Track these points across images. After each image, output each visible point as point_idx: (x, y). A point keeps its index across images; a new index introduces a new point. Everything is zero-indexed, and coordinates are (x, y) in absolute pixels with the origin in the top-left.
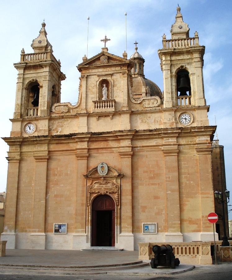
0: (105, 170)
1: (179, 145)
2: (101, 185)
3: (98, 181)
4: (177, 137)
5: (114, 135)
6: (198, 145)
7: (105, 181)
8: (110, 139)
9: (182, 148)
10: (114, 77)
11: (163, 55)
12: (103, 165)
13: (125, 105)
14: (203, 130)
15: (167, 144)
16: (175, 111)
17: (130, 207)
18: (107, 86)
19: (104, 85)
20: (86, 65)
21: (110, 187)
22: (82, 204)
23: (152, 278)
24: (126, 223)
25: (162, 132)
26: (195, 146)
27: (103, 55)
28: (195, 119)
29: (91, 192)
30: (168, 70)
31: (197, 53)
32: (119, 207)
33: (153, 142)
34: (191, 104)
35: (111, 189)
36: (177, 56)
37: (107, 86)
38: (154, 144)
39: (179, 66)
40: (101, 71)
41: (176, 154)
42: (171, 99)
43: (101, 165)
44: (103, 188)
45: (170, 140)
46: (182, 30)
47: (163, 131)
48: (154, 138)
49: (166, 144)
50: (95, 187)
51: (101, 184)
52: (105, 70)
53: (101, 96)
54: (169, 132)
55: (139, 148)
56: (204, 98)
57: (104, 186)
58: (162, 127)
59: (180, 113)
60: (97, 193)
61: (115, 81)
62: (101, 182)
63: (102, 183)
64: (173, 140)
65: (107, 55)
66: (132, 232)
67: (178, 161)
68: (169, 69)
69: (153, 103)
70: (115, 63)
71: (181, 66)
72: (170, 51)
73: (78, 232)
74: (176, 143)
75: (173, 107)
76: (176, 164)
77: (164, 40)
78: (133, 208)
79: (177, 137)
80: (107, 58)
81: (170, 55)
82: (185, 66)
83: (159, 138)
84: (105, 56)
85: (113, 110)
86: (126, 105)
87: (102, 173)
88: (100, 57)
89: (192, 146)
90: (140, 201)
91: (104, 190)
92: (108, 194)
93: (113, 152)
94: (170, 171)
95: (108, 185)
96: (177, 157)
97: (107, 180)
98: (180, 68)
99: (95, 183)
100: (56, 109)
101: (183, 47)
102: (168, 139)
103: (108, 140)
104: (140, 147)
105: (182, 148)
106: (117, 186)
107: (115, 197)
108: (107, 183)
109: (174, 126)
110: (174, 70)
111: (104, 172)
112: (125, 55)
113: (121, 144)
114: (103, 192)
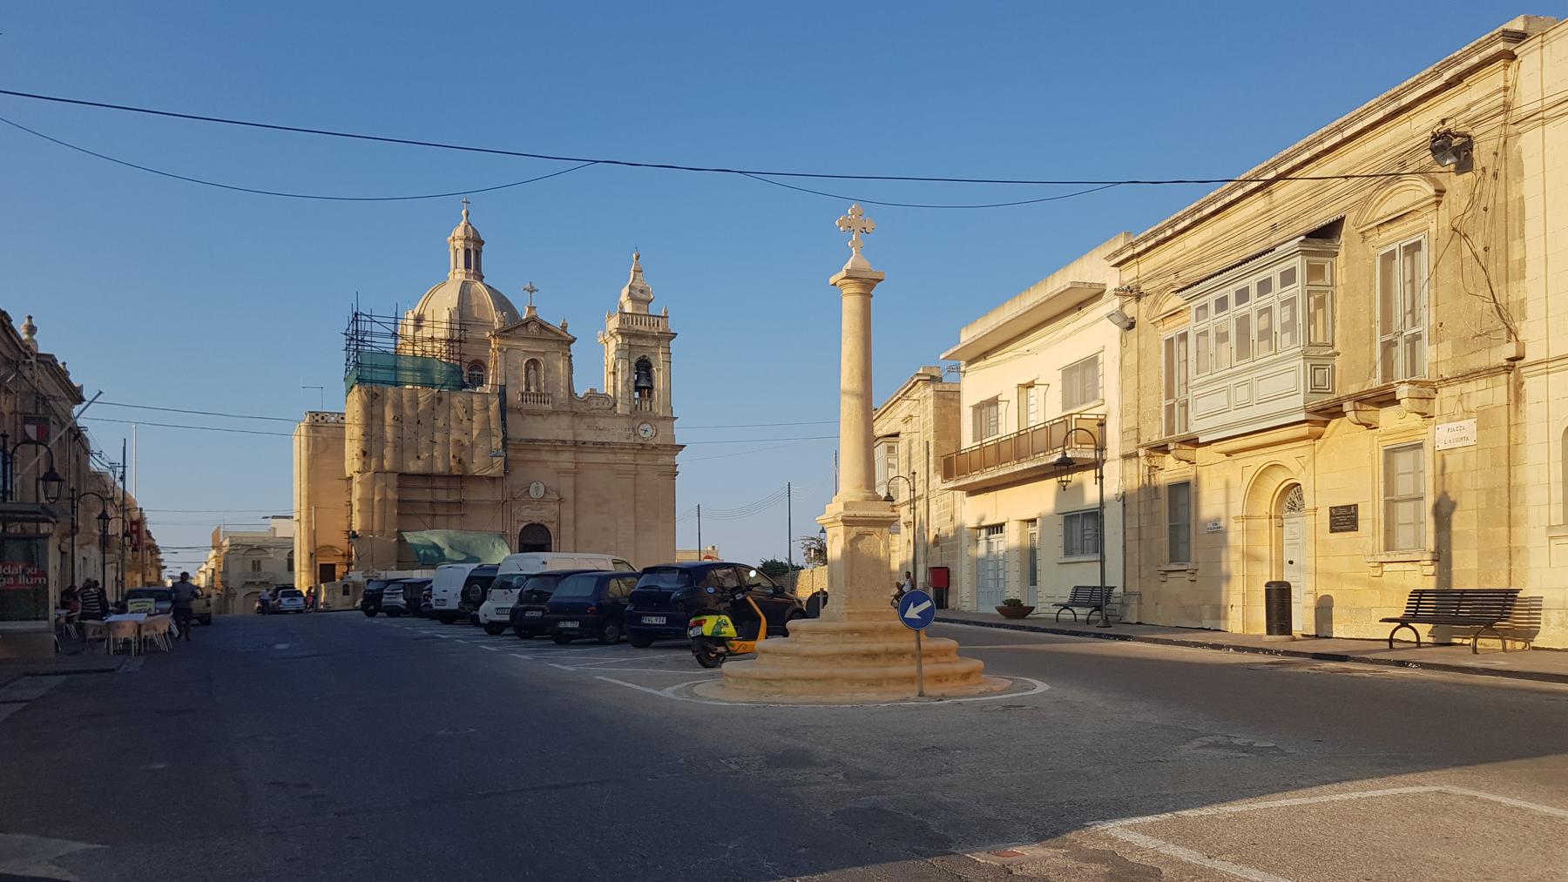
1: (637, 465)
4: (635, 454)
7: (539, 507)
19: (532, 367)
20: (505, 331)
21: (547, 514)
46: (643, 296)
52: (534, 343)
59: (639, 422)
64: (628, 458)
70: (552, 336)
79: (635, 454)
85: (551, 408)
92: (543, 523)
101: (648, 329)
107: (552, 528)
110: (634, 361)
114: (536, 520)
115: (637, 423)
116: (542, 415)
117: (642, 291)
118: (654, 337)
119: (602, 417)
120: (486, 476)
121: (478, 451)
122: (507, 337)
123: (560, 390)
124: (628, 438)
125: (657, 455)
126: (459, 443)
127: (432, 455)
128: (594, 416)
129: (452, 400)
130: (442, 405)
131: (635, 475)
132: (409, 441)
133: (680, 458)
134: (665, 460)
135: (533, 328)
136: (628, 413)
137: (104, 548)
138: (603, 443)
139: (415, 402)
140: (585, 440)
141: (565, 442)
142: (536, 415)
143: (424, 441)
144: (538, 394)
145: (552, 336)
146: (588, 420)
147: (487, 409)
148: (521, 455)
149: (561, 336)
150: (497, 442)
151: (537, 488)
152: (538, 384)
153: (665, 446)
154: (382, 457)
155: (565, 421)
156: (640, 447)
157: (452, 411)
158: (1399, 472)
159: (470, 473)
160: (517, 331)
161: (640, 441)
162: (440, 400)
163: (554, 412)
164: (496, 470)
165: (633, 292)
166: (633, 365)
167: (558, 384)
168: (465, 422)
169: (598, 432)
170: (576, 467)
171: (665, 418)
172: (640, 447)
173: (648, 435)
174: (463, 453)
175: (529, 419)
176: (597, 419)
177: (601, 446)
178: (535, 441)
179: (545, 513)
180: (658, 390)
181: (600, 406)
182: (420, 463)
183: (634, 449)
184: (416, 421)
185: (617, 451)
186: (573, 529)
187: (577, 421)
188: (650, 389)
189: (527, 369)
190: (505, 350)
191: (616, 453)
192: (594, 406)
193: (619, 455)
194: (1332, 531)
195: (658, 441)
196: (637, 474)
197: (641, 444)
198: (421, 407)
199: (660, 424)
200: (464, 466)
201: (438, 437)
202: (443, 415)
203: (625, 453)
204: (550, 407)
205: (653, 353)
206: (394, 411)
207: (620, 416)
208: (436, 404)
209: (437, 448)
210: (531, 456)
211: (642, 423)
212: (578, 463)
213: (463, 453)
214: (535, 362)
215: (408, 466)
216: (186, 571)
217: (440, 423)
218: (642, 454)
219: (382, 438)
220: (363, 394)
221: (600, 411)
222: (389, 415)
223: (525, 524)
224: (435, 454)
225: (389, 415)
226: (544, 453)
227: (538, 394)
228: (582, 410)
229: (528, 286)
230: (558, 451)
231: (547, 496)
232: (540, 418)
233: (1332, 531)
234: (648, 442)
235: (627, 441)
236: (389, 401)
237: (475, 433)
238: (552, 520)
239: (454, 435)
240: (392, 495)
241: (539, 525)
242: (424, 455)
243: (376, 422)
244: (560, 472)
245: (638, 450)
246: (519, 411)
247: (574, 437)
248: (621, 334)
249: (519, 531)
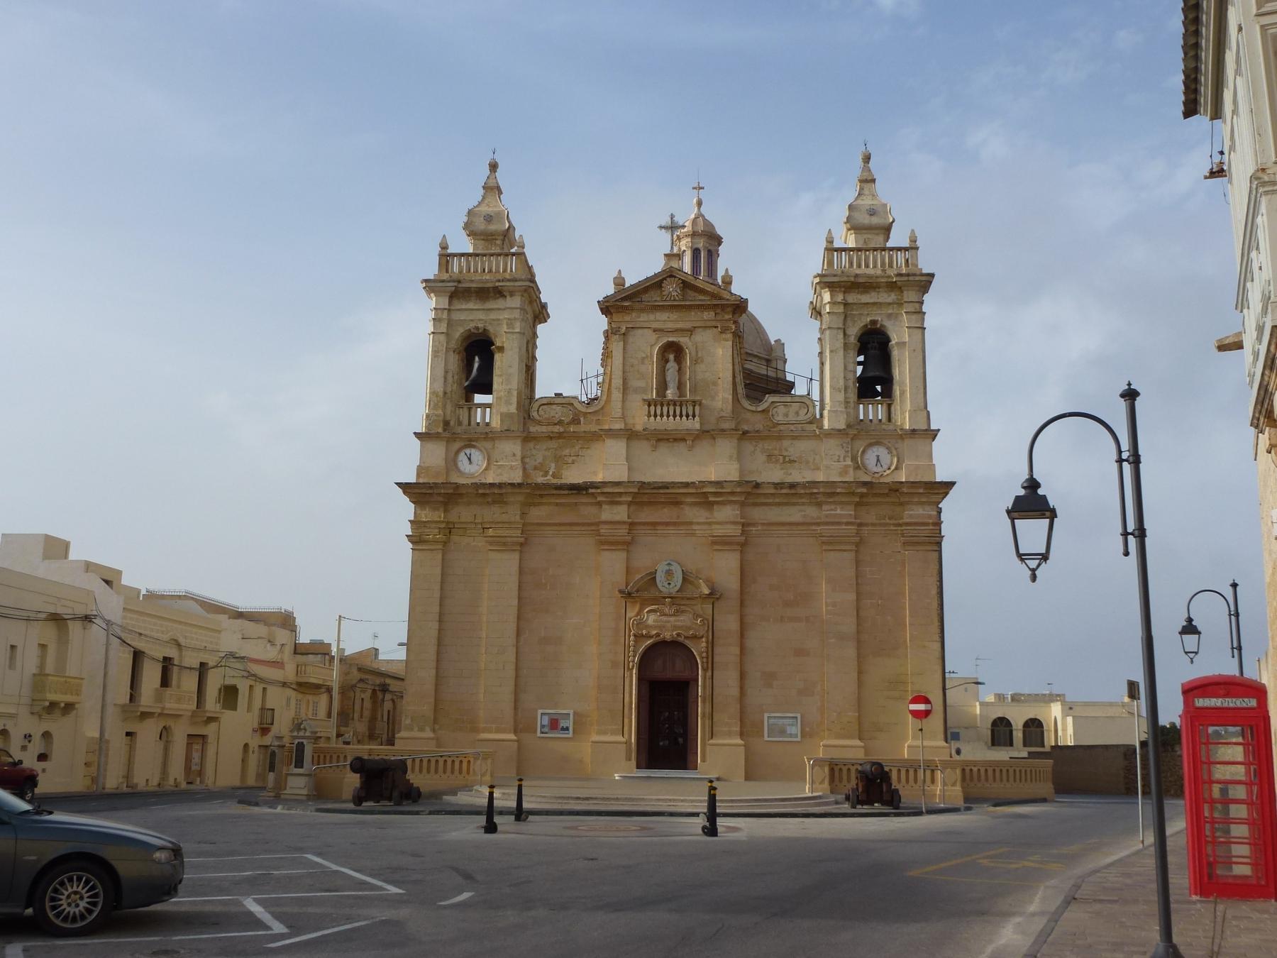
1: (860, 525)
19: (671, 357)
22: (614, 664)
24: (727, 717)
40: (665, 319)
43: (667, 568)
69: (797, 413)
73: (605, 733)
79: (858, 505)
85: (697, 426)
87: (667, 586)
92: (681, 639)
93: (693, 535)
100: (541, 412)
107: (698, 649)
110: (854, 330)
111: (673, 585)
115: (860, 445)
116: (684, 440)
124: (844, 471)
125: (902, 504)
128: (780, 438)
133: (948, 505)
134: (917, 512)
135: (671, 288)
137: (201, 770)
142: (675, 440)
146: (768, 445)
155: (726, 447)
156: (864, 490)
158: (1237, 673)
160: (645, 297)
161: (867, 479)
170: (743, 532)
172: (864, 490)
176: (786, 443)
177: (791, 492)
181: (792, 417)
183: (853, 494)
186: (737, 650)
187: (748, 447)
189: (663, 360)
190: (623, 330)
193: (825, 507)
194: (38, 761)
197: (865, 484)
203: (834, 503)
211: (871, 445)
212: (749, 525)
229: (696, 185)
233: (38, 761)
248: (831, 286)
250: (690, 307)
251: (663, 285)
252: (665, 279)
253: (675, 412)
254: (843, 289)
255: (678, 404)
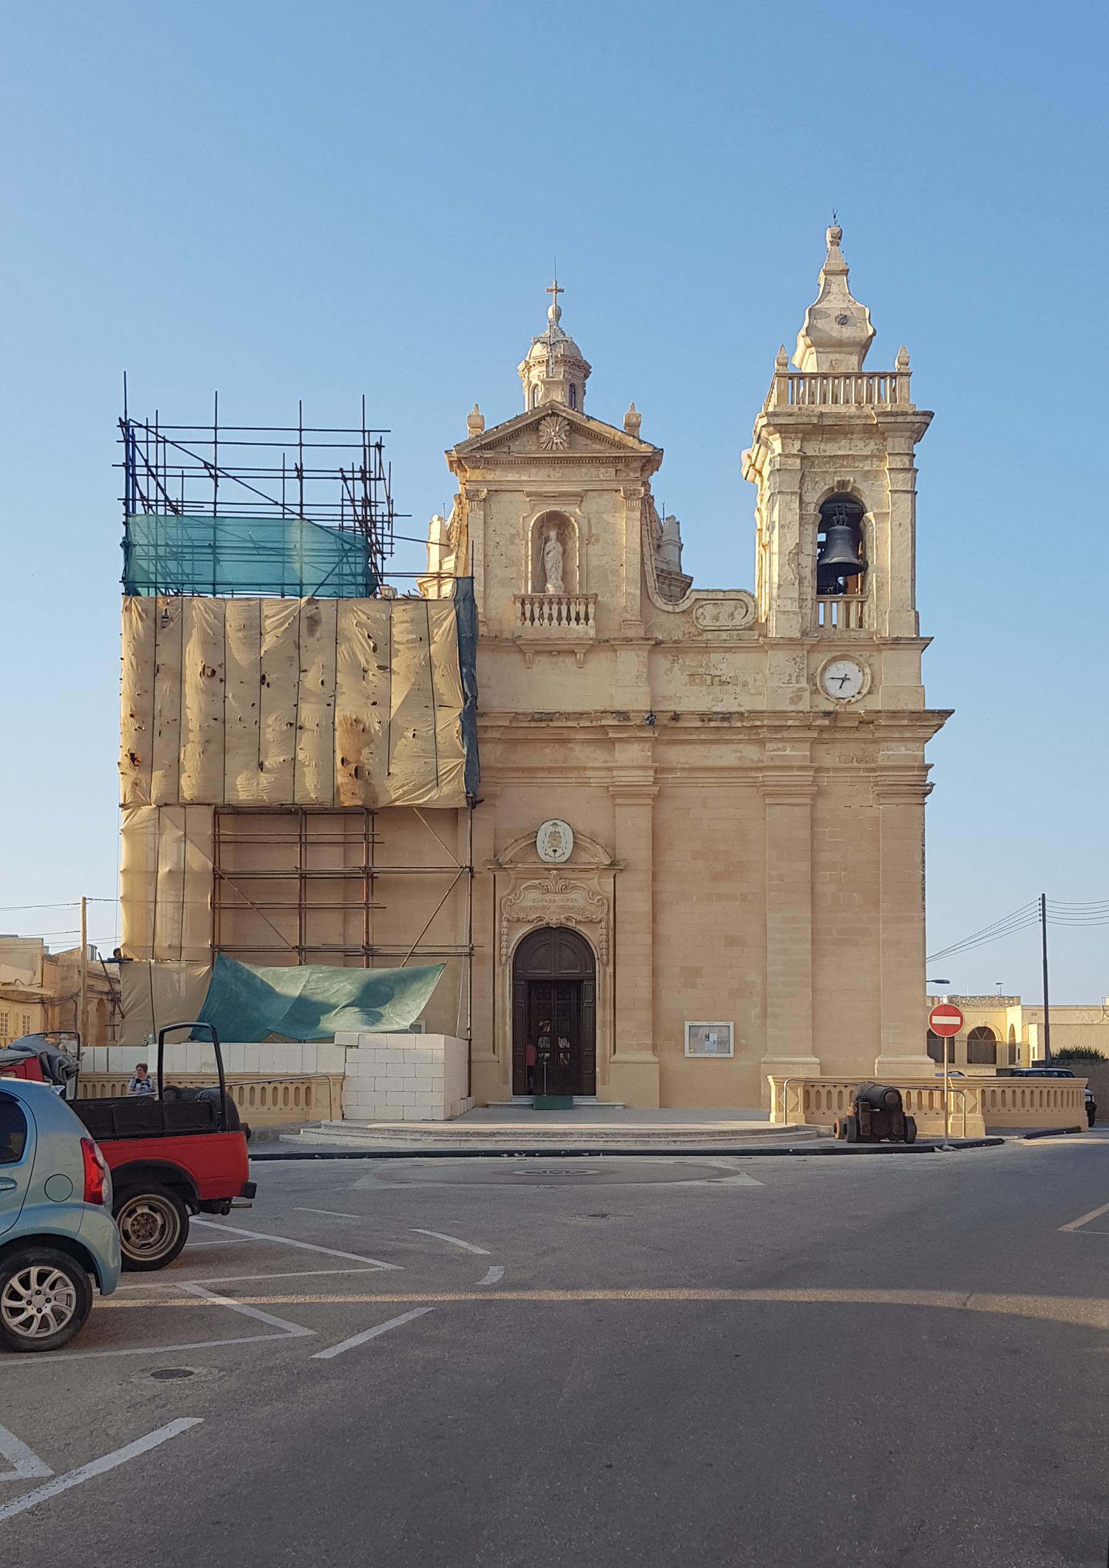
0: (563, 845)
1: (818, 770)
2: (548, 897)
3: (537, 882)
4: (814, 742)
5: (595, 724)
6: (884, 773)
7: (561, 882)
8: (579, 736)
9: (824, 778)
10: (591, 505)
11: (778, 435)
12: (558, 829)
13: (629, 617)
14: (905, 722)
15: (778, 764)
16: (813, 649)
17: (646, 971)
18: (562, 539)
19: (553, 534)
20: (482, 447)
21: (581, 903)
23: (752, 1150)
25: (766, 722)
26: (872, 774)
27: (554, 414)
28: (877, 682)
29: (510, 918)
30: (793, 493)
31: (902, 437)
32: (610, 969)
33: (726, 755)
34: (866, 625)
35: (582, 910)
36: (828, 440)
37: (562, 539)
38: (734, 762)
39: (832, 481)
41: (808, 801)
42: (796, 604)
43: (552, 829)
44: (553, 907)
45: (788, 752)
46: (847, 332)
47: (769, 718)
48: (731, 742)
49: (773, 764)
50: (527, 903)
51: (548, 891)
52: (556, 474)
53: (541, 577)
54: (790, 723)
55: (678, 775)
56: (914, 608)
57: (558, 897)
58: (761, 704)
59: (829, 656)
60: (532, 922)
61: (594, 521)
62: (548, 884)
63: (551, 887)
64: (796, 753)
65: (565, 418)
66: (653, 1052)
67: (813, 822)
68: (797, 490)
70: (598, 449)
71: (838, 481)
72: (805, 420)
74: (808, 763)
75: (804, 633)
76: (805, 834)
77: (782, 370)
78: (655, 973)
79: (814, 742)
80: (568, 428)
81: (800, 435)
82: (855, 481)
83: (749, 741)
84: (560, 419)
85: (592, 633)
86: (633, 615)
87: (552, 854)
88: (538, 422)
89: (862, 774)
90: (94, 1242)
91: (559, 914)
92: (572, 924)
94: (303, 963)
95: (573, 896)
96: (809, 808)
97: (571, 879)
98: (836, 490)
99: (527, 888)
101: (853, 409)
102: (780, 745)
103: (570, 741)
104: (683, 769)
105: (824, 778)
106: (605, 901)
107: (595, 936)
108: (564, 889)
109: (803, 705)
110: (815, 497)
111: (557, 854)
112: (634, 420)
113: (617, 755)
114: (554, 918)
117: (843, 320)
118: (870, 431)
119: (729, 650)
120: (420, 808)
121: (404, 745)
122: (487, 461)
123: (618, 587)
124: (796, 698)
125: (875, 741)
126: (357, 726)
127: (294, 759)
128: (706, 649)
129: (343, 623)
130: (318, 635)
131: (814, 797)
132: (240, 726)
133: (935, 749)
134: (897, 752)
135: (551, 431)
136: (798, 635)
138: (726, 717)
139: (254, 630)
140: (679, 708)
141: (623, 715)
143: (273, 727)
144: (566, 598)
145: (598, 449)
146: (691, 661)
147: (426, 639)
148: (525, 757)
149: (619, 445)
150: (449, 722)
151: (555, 836)
152: (565, 576)
153: (894, 714)
154: (177, 767)
155: (630, 662)
156: (826, 722)
157: (343, 649)
159: (383, 801)
160: (515, 446)
161: (830, 707)
162: (314, 622)
163: (603, 644)
164: (446, 789)
165: (820, 323)
166: (812, 510)
167: (616, 573)
168: (373, 673)
169: (717, 689)
171: (896, 642)
173: (849, 690)
174: (365, 752)
175: (542, 664)
176: (715, 657)
178: (549, 717)
179: (577, 898)
180: (881, 570)
181: (724, 621)
182: (264, 779)
183: (809, 727)
184: (258, 677)
185: (764, 734)
186: (648, 939)
187: (663, 663)
188: (857, 569)
191: (762, 742)
192: (707, 622)
193: (769, 746)
195: (877, 703)
196: (818, 794)
197: (827, 714)
198: (269, 642)
199: (886, 660)
200: (368, 784)
201: (309, 713)
202: (319, 660)
204: (588, 630)
205: (866, 475)
206: (205, 653)
207: (775, 645)
208: (304, 632)
209: (306, 740)
210: (549, 755)
211: (834, 660)
213: (365, 752)
214: (556, 522)
215: (234, 788)
216: (115, 948)
217: (311, 680)
218: (834, 741)
219: (178, 722)
220: (135, 615)
221: (724, 635)
222: (194, 660)
223: (526, 929)
224: (301, 756)
225: (194, 660)
226: (577, 748)
227: (566, 598)
228: (677, 635)
230: (613, 741)
231: (584, 857)
232: (569, 660)
234: (849, 708)
235: (792, 708)
236: (195, 631)
237: (397, 701)
238: (597, 917)
239: (347, 707)
240: (199, 860)
241: (563, 930)
242: (274, 759)
243: (164, 686)
244: (616, 794)
245: (821, 729)
246: (517, 645)
247: (654, 702)
248: (782, 430)
249: (513, 944)
250: (579, 461)
251: (541, 427)
252: (543, 418)
253: (560, 613)
254: (800, 435)
255: (555, 600)
